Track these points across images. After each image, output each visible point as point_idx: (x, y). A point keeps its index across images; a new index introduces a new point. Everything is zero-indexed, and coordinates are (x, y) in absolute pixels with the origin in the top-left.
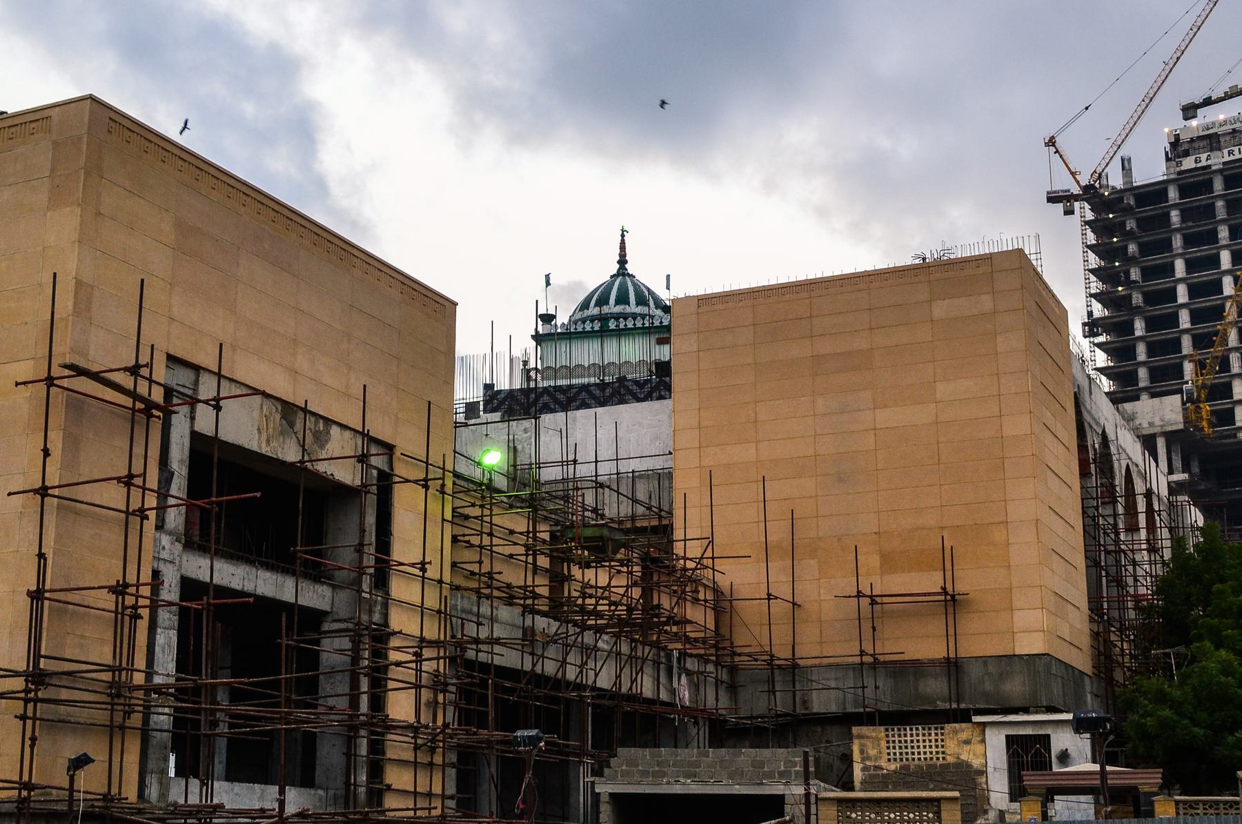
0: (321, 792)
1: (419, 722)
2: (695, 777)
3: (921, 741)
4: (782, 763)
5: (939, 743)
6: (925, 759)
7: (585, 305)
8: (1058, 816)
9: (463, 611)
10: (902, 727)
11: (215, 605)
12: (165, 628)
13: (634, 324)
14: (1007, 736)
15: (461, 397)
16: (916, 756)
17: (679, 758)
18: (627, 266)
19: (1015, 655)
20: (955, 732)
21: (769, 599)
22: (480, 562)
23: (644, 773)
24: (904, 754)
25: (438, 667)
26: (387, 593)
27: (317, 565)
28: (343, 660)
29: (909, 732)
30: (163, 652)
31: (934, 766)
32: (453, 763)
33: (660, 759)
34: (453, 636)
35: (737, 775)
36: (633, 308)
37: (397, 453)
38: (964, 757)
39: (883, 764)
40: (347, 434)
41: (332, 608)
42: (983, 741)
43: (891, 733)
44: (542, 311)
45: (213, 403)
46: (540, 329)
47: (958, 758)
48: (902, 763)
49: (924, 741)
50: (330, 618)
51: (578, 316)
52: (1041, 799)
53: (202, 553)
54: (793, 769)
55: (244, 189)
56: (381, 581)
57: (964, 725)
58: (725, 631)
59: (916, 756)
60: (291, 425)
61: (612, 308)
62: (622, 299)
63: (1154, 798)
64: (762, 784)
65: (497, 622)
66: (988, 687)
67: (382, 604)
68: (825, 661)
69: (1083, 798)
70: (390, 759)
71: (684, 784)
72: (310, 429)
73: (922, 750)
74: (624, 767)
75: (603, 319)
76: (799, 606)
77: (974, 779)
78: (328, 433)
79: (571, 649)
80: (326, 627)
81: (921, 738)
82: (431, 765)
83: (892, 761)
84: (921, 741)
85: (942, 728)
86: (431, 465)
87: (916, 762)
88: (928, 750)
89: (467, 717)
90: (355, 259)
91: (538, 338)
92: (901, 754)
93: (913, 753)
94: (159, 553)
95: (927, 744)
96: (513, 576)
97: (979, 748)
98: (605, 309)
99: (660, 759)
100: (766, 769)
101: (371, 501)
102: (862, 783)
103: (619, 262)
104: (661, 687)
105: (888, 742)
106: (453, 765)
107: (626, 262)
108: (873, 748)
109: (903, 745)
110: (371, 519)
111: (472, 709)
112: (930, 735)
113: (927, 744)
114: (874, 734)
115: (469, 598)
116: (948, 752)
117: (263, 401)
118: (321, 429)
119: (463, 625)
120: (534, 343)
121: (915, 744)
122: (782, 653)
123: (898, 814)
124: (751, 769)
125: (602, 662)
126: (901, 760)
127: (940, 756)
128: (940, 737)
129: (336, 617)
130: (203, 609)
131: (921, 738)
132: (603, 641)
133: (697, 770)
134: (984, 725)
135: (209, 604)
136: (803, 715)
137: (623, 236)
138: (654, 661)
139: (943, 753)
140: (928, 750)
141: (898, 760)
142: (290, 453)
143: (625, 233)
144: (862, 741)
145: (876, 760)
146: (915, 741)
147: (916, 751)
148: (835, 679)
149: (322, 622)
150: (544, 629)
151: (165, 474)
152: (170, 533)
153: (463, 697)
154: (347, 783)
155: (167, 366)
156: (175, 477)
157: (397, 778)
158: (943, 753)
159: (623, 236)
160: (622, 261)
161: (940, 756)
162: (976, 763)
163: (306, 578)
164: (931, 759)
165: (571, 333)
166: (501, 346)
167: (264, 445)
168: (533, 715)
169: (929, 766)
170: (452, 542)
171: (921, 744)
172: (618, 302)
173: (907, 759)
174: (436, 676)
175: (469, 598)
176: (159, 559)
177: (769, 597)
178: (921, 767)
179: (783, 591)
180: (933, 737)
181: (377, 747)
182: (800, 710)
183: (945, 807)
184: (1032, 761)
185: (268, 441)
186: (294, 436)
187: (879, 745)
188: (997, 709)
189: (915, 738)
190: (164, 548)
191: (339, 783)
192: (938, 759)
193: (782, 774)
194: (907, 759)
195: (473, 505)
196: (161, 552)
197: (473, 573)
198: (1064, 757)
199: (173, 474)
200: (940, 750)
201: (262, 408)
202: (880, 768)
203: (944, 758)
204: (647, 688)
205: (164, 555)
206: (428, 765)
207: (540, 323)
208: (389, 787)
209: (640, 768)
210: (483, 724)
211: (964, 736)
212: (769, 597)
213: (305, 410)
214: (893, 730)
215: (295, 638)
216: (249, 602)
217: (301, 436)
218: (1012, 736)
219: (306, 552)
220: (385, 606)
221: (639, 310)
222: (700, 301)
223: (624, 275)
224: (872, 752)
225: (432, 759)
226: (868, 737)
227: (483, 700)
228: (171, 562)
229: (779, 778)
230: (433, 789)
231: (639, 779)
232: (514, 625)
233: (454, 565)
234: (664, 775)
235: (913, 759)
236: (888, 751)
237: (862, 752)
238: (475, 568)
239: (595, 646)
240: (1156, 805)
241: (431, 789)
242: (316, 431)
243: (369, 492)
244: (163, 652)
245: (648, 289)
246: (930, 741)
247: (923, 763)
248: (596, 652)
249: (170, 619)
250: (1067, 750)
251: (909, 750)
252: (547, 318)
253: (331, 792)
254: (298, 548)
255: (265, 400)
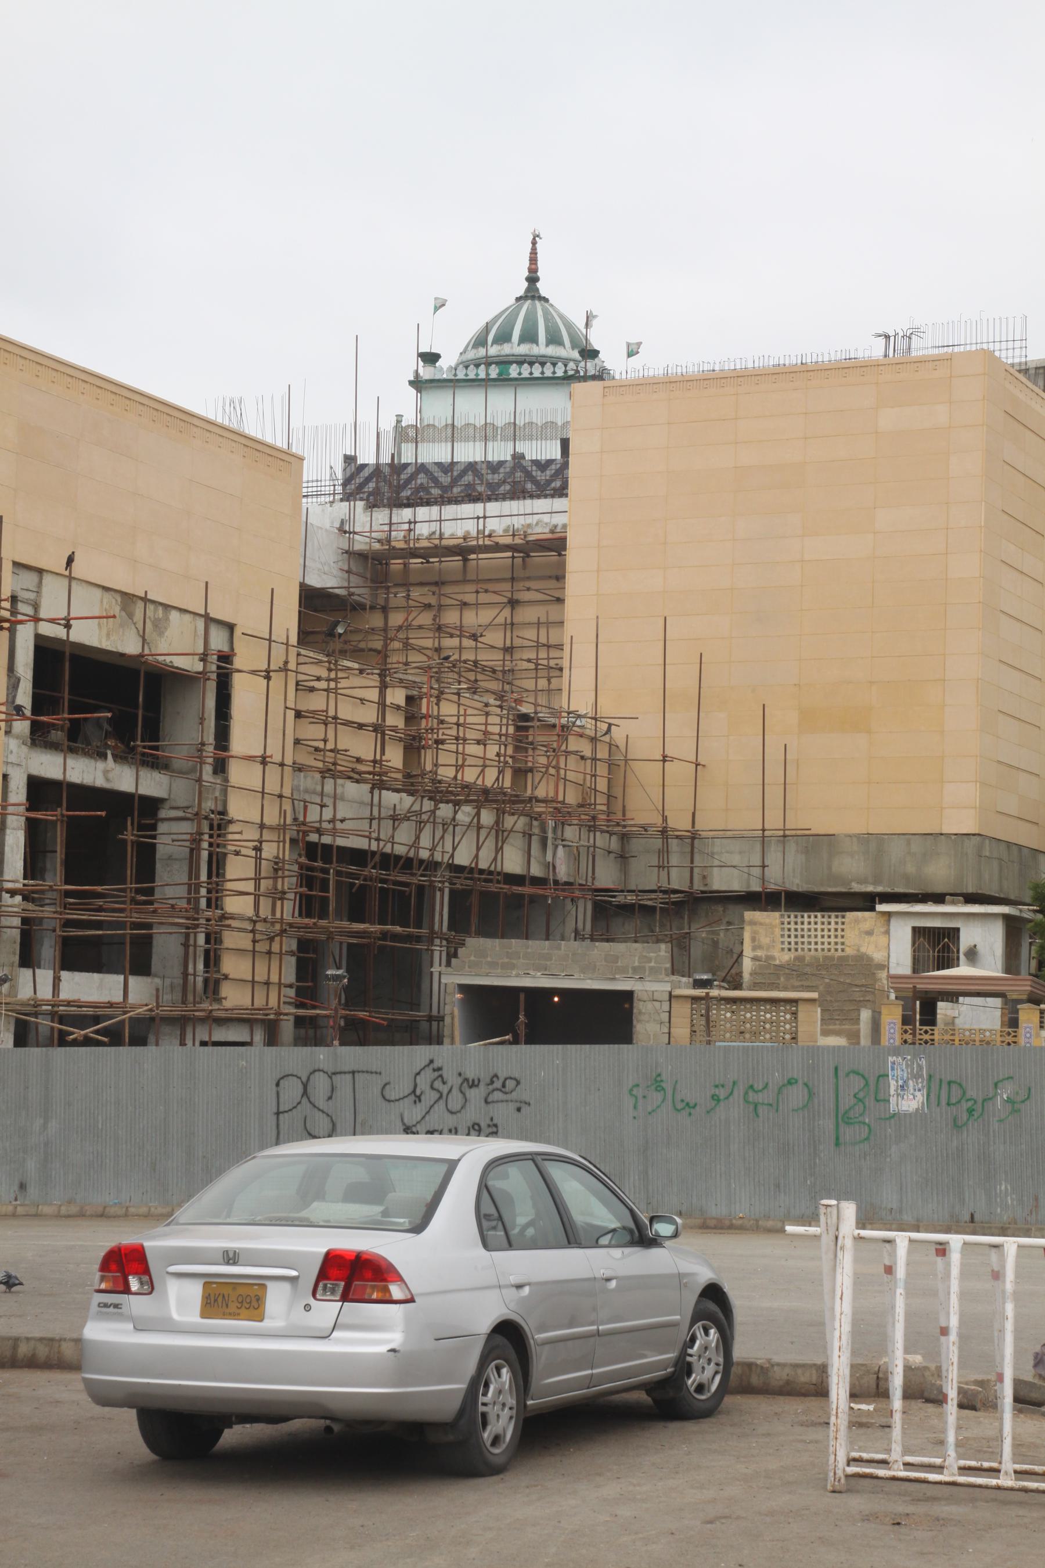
0: (157, 981)
1: (257, 915)
2: (546, 970)
3: (819, 929)
4: (637, 958)
5: (839, 933)
6: (823, 950)
7: (480, 341)
8: (961, 1017)
9: (306, 791)
10: (799, 914)
11: (68, 817)
12: (14, 829)
13: (543, 373)
14: (914, 929)
15: (315, 478)
16: (813, 946)
17: (529, 950)
18: (539, 285)
19: (942, 834)
20: (857, 921)
21: (664, 761)
22: (325, 741)
23: (493, 965)
24: (799, 943)
25: (278, 853)
26: (226, 780)
27: (157, 757)
28: (182, 851)
29: (806, 920)
30: (12, 851)
31: (832, 958)
32: (292, 951)
33: (510, 951)
34: (295, 819)
35: (589, 969)
36: (541, 349)
37: (238, 632)
38: (863, 950)
39: (776, 953)
40: (187, 617)
41: (169, 795)
42: (887, 932)
43: (799, 920)
44: (424, 349)
45: (63, 622)
46: (421, 371)
47: (858, 950)
48: (797, 954)
49: (823, 930)
50: (167, 805)
51: (471, 355)
52: (902, 1003)
53: (44, 750)
54: (647, 965)
55: (83, 376)
56: (221, 767)
57: (867, 914)
58: (618, 792)
59: (813, 946)
60: (131, 616)
61: (515, 348)
62: (529, 336)
63: (1019, 1006)
64: (614, 979)
65: (342, 799)
66: (910, 869)
67: (221, 790)
68: (729, 834)
69: (990, 1001)
70: (227, 949)
71: (534, 977)
72: (150, 618)
73: (819, 940)
74: (472, 958)
75: (504, 362)
76: (704, 766)
77: (874, 974)
78: (167, 619)
79: (424, 826)
80: (163, 813)
81: (819, 926)
82: (269, 953)
83: (786, 950)
84: (819, 929)
85: (843, 917)
86: (274, 641)
87: (813, 952)
88: (826, 940)
89: (309, 906)
90: (195, 429)
91: (418, 384)
92: (796, 943)
93: (810, 943)
94: (7, 757)
95: (826, 933)
96: (362, 747)
97: (883, 940)
98: (506, 349)
99: (510, 951)
100: (619, 964)
101: (211, 688)
102: (751, 974)
103: (528, 279)
104: (532, 860)
105: (783, 929)
106: (291, 953)
107: (537, 279)
108: (766, 936)
109: (799, 933)
110: (211, 703)
111: (314, 895)
112: (829, 923)
113: (826, 933)
114: (767, 921)
115: (313, 777)
116: (847, 943)
117: (102, 596)
118: (161, 616)
119: (305, 808)
120: (415, 392)
121: (813, 933)
122: (680, 822)
123: (754, 1013)
124: (604, 963)
125: (460, 837)
126: (796, 950)
127: (839, 947)
128: (840, 926)
129: (174, 805)
130: (58, 820)
131: (819, 926)
132: (463, 812)
133: (548, 963)
134: (889, 915)
135: (63, 815)
136: (703, 892)
137: (534, 243)
138: (524, 833)
139: (843, 944)
140: (826, 940)
141: (793, 950)
142: (130, 646)
143: (537, 239)
144: (755, 928)
145: (768, 949)
146: (813, 930)
147: (813, 940)
148: (740, 853)
149: (158, 809)
150: (395, 805)
151: (13, 680)
152: (17, 737)
153: (304, 882)
154: (185, 974)
155: (13, 572)
156: (21, 681)
157: (233, 966)
158: (843, 944)
159: (534, 243)
160: (533, 279)
161: (839, 947)
162: (878, 956)
163: (143, 766)
164: (829, 950)
165: (458, 381)
166: (367, 417)
167: (104, 640)
168: (377, 903)
169: (826, 958)
170: (295, 717)
171: (819, 933)
172: (523, 340)
173: (803, 949)
174: (276, 863)
175: (313, 777)
176: (7, 763)
177: (665, 759)
178: (817, 959)
179: (681, 747)
180: (833, 926)
181: (213, 938)
182: (698, 886)
183: (803, 1010)
184: (938, 956)
185: (108, 635)
186: (133, 627)
187: (773, 933)
188: (916, 895)
189: (813, 926)
190: (11, 752)
191: (177, 971)
192: (836, 950)
193: (635, 970)
194: (803, 949)
195: (319, 679)
196: (10, 756)
197: (317, 749)
198: (972, 954)
199: (19, 680)
200: (839, 940)
201: (102, 602)
202: (773, 958)
203: (843, 950)
204: (512, 862)
205: (12, 758)
206: (267, 953)
207: (421, 363)
208: (226, 977)
209: (489, 959)
210: (323, 914)
211: (866, 926)
212: (665, 759)
213: (145, 600)
214: (789, 917)
215: (135, 832)
216: (101, 816)
217: (140, 626)
218: (919, 928)
219: (144, 747)
220: (225, 792)
221: (552, 351)
222: (606, 390)
223: (533, 298)
224: (765, 940)
225: (270, 947)
226: (761, 924)
227: (324, 886)
228: (18, 765)
229: (633, 973)
230: (271, 977)
231: (487, 971)
232: (362, 803)
233: (297, 742)
234: (513, 967)
235: (810, 950)
236: (782, 940)
237: (753, 939)
238: (321, 745)
239: (454, 819)
240: (1020, 1012)
241: (269, 978)
242: (155, 619)
243: (209, 679)
244: (12, 851)
245: (562, 317)
246: (829, 930)
247: (820, 954)
248: (454, 826)
249: (17, 820)
250: (975, 946)
251: (806, 940)
252: (430, 358)
253: (168, 981)
254: (139, 743)
255: (105, 593)
